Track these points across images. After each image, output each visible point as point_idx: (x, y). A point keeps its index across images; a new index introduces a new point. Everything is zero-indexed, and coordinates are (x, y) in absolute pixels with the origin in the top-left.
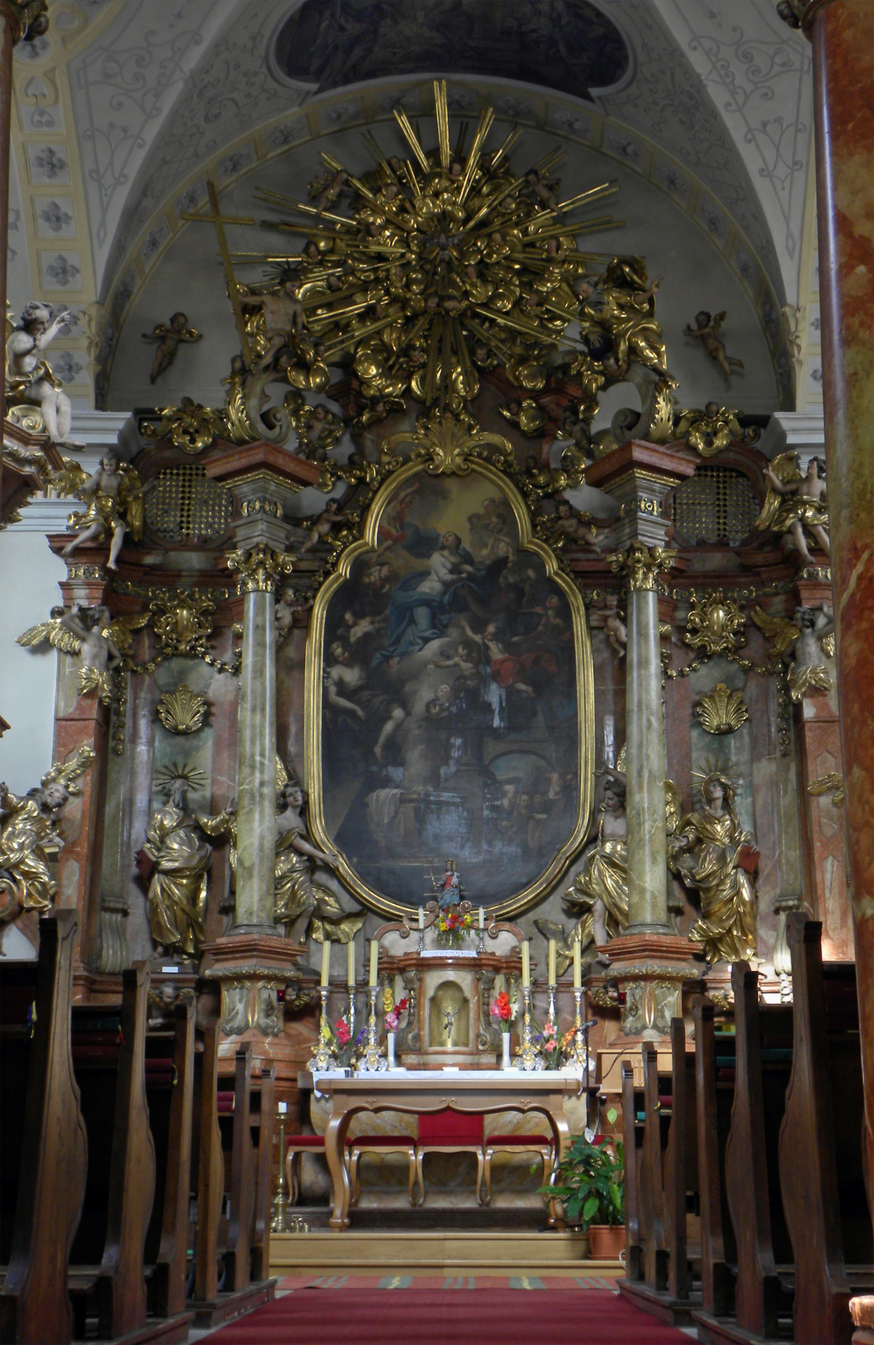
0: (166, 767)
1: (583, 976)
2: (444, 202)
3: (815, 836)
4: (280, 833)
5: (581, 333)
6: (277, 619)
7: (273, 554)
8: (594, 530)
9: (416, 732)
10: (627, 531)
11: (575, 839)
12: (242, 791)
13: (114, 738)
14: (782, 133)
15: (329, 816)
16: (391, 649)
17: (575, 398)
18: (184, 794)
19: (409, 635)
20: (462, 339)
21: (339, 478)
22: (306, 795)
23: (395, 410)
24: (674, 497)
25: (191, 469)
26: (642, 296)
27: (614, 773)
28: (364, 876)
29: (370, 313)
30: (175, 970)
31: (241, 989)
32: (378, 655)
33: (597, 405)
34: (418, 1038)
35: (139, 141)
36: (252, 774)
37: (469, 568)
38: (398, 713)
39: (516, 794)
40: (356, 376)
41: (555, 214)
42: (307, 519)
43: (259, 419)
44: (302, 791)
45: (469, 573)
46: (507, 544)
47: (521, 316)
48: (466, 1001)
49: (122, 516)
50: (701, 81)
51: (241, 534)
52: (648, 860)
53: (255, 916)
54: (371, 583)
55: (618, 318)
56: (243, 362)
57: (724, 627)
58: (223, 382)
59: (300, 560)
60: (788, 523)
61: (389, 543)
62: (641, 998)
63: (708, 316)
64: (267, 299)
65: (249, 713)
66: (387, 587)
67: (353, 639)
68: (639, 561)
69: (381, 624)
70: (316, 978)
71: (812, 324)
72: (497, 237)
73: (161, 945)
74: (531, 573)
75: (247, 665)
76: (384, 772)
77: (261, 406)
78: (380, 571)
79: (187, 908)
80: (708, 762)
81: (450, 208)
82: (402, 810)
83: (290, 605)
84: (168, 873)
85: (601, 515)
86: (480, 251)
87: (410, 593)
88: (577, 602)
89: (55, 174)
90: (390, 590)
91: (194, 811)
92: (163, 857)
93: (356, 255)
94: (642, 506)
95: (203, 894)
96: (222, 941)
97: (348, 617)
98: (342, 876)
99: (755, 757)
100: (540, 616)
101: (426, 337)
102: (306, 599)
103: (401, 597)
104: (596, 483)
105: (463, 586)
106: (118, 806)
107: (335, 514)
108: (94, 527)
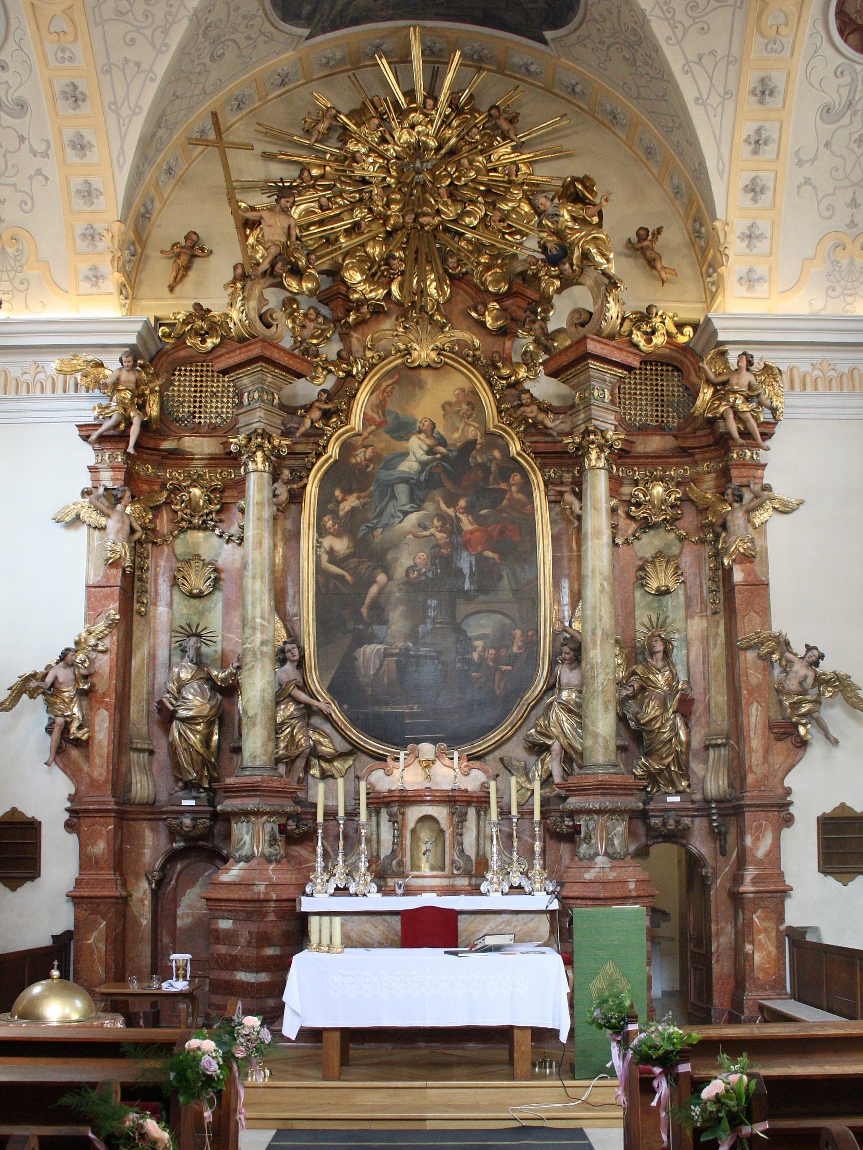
0: (182, 628)
1: (542, 806)
2: (419, 133)
3: (743, 685)
4: (280, 685)
5: (539, 242)
6: (275, 496)
7: (270, 438)
8: (551, 416)
9: (397, 595)
10: (582, 416)
11: (536, 688)
12: (245, 649)
13: (138, 602)
14: (716, 64)
15: (322, 668)
16: (375, 521)
17: (534, 301)
18: (198, 649)
19: (390, 509)
20: (436, 251)
21: (330, 372)
22: (301, 650)
23: (378, 311)
24: (619, 387)
25: (202, 366)
26: (593, 210)
27: (569, 630)
28: (353, 723)
29: (355, 229)
30: (192, 803)
31: (248, 822)
32: (363, 527)
33: (552, 308)
34: (401, 864)
35: (151, 75)
36: (254, 634)
37: (442, 449)
38: (381, 578)
39: (484, 649)
40: (345, 283)
41: (514, 143)
42: (301, 407)
43: (257, 318)
44: (299, 647)
45: (442, 454)
46: (476, 428)
47: (486, 231)
48: (442, 832)
49: (141, 408)
50: (645, 17)
51: (243, 420)
52: (600, 708)
53: (258, 759)
54: (357, 463)
55: (571, 229)
56: (243, 268)
57: (664, 502)
58: (226, 287)
59: (295, 443)
60: (721, 409)
61: (373, 427)
62: (594, 829)
63: (647, 230)
64: (265, 214)
65: (250, 580)
66: (372, 466)
67: (341, 513)
68: (593, 443)
69: (366, 500)
70: (313, 810)
71: (739, 237)
72: (465, 162)
73: (181, 780)
74: (497, 454)
75: (248, 538)
76: (370, 630)
77: (259, 309)
78: (365, 453)
79: (201, 751)
80: (650, 620)
81: (423, 139)
82: (386, 663)
83: (286, 483)
84: (184, 720)
85: (555, 403)
86: (450, 175)
87: (392, 472)
88: (537, 480)
89: (79, 106)
90: (374, 469)
91: (207, 665)
92: (179, 706)
93: (343, 179)
94: (596, 394)
95: (216, 737)
96: (230, 781)
97: (338, 493)
98: (334, 721)
99: (688, 616)
100: (505, 492)
101: (404, 249)
102: (301, 478)
103: (383, 475)
104: (553, 374)
105: (437, 466)
106: (143, 660)
107: (326, 403)
108: (115, 417)
